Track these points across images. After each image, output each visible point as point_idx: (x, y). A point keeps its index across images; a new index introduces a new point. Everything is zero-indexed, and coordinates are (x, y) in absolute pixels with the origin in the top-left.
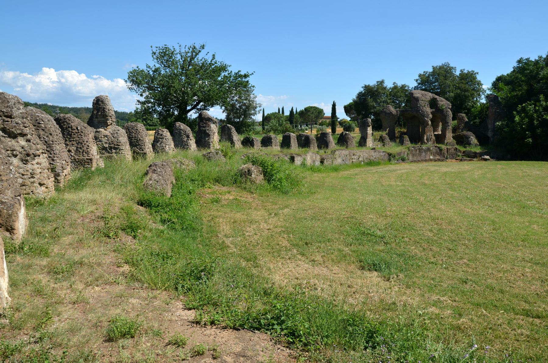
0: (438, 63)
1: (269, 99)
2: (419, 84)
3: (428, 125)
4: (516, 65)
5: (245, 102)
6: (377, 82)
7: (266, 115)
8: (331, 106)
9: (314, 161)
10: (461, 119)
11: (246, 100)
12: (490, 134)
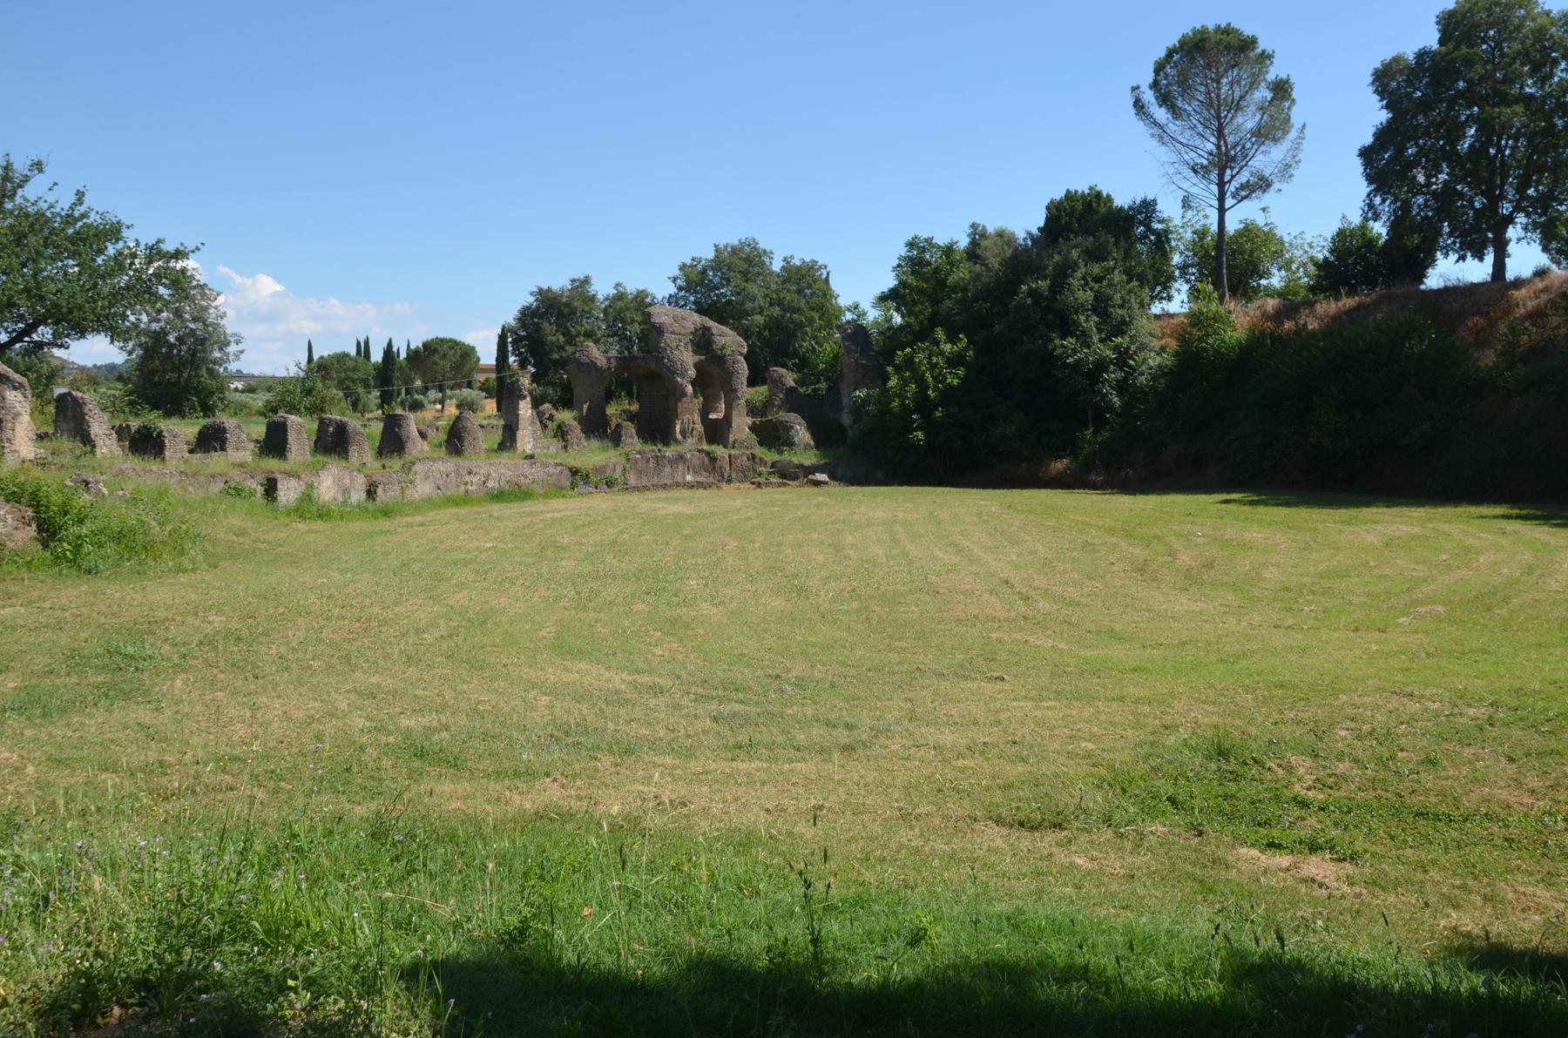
0: (731, 237)
1: (271, 324)
2: (680, 289)
3: (685, 395)
4: (903, 251)
5: (192, 326)
6: (573, 281)
7: (316, 357)
8: (496, 339)
9: (346, 491)
10: (778, 383)
11: (195, 320)
12: (846, 420)
